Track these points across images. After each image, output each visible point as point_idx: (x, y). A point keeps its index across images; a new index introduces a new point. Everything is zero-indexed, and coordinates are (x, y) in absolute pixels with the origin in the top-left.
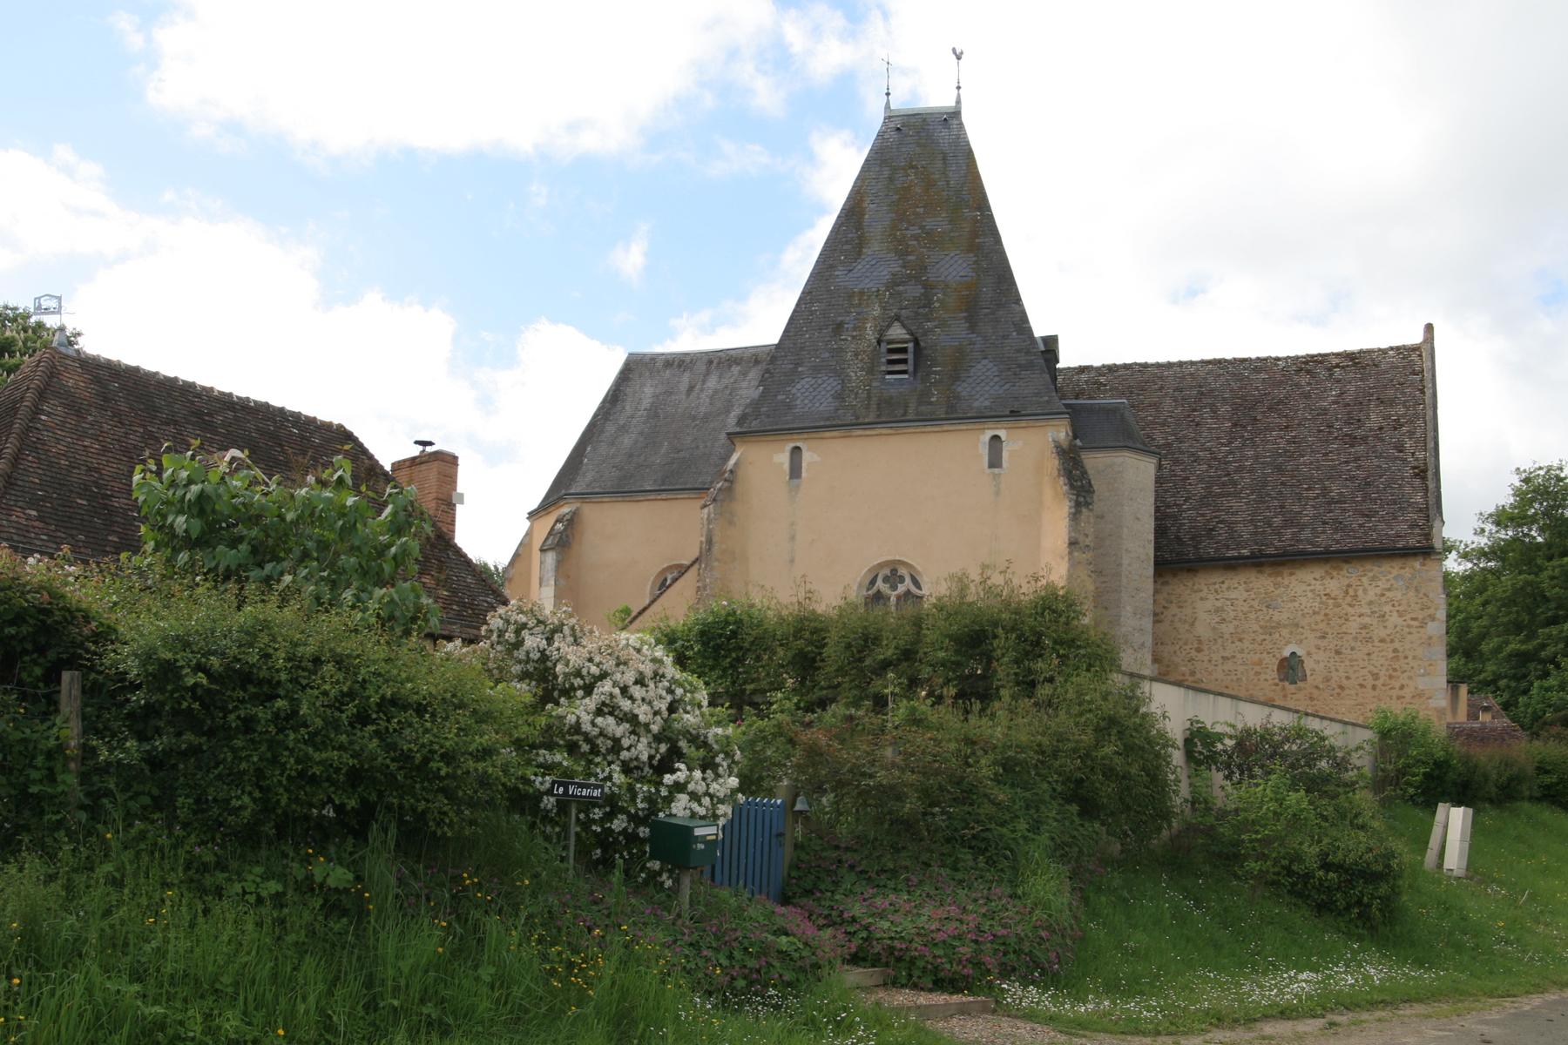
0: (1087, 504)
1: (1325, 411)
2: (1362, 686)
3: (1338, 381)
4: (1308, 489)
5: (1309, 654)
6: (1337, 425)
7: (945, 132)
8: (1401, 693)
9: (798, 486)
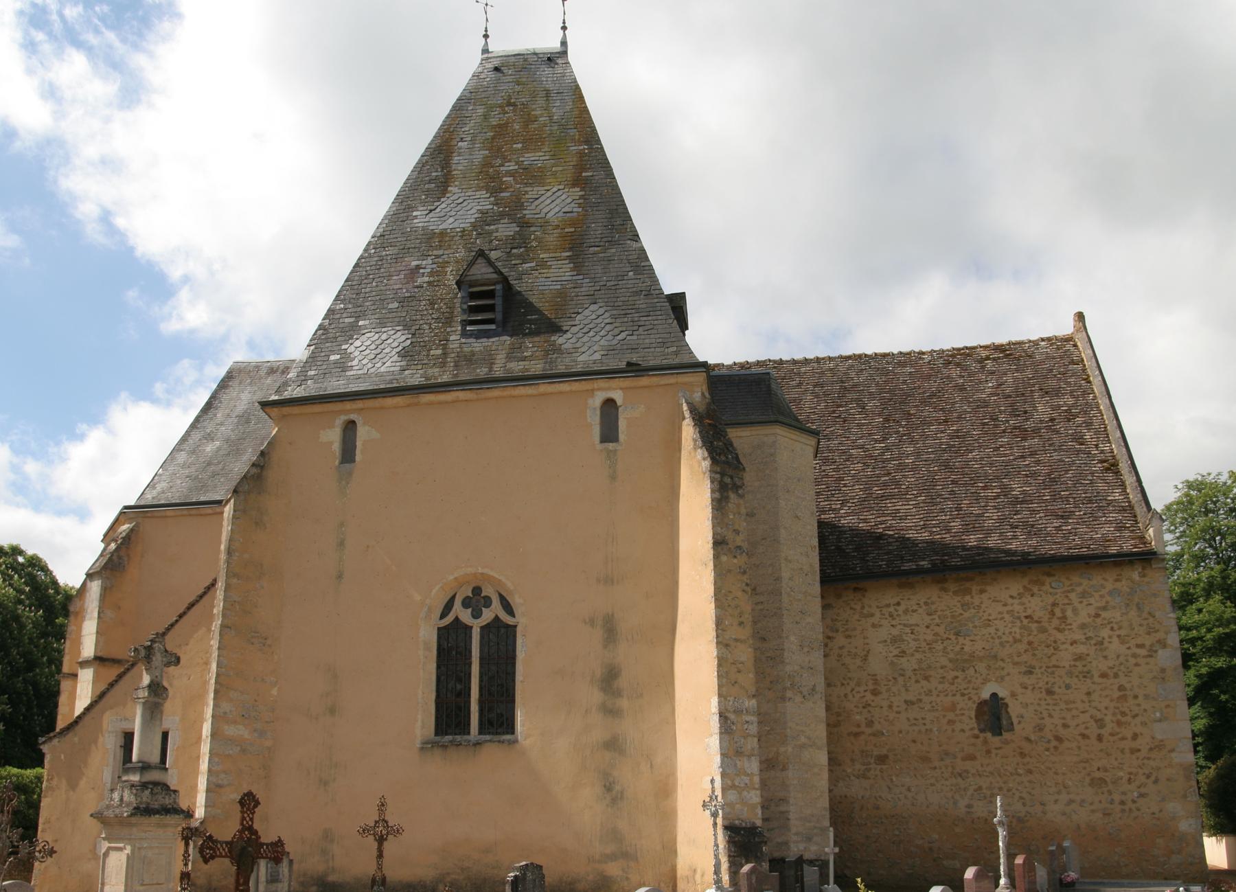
0: (736, 488)
1: (985, 404)
2: (1084, 736)
3: (993, 373)
4: (985, 488)
5: (1013, 695)
6: (1002, 417)
7: (548, 71)
8: (1134, 745)
9: (350, 474)
